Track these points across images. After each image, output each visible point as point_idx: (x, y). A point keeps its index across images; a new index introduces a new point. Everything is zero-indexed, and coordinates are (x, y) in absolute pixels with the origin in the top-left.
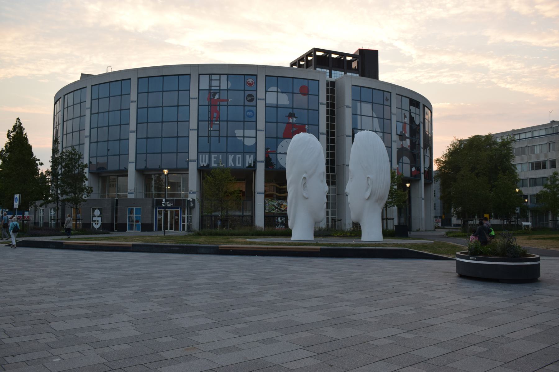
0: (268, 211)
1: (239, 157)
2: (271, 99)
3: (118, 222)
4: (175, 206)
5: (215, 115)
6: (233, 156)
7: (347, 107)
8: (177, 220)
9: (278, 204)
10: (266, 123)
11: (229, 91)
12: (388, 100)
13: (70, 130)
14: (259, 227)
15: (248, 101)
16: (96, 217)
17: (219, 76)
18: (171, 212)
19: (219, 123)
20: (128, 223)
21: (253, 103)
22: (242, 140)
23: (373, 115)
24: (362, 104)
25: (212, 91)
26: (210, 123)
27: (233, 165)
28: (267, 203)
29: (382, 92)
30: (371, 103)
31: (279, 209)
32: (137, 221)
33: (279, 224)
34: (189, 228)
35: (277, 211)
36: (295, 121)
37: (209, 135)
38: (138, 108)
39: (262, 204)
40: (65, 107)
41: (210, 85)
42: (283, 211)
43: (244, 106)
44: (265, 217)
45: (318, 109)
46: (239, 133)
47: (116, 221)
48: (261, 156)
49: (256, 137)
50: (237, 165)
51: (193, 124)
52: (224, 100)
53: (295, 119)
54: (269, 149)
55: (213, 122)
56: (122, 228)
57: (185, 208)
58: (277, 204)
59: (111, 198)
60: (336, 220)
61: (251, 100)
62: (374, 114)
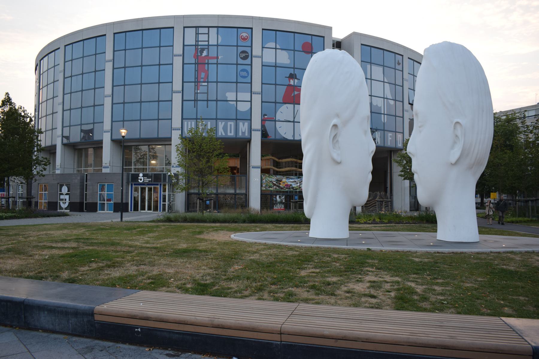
0: (264, 189)
1: (231, 125)
2: (269, 57)
3: (88, 201)
4: (154, 182)
5: (203, 75)
6: (223, 123)
8: (156, 199)
9: (276, 180)
10: (263, 103)
11: (219, 47)
13: (45, 99)
14: (254, 209)
15: (241, 58)
16: (63, 195)
17: (207, 29)
18: (150, 189)
19: (208, 84)
20: (98, 202)
21: (248, 61)
22: (234, 104)
23: (384, 80)
25: (199, 47)
26: (196, 84)
27: (224, 134)
28: (264, 179)
29: (394, 54)
30: (382, 66)
31: (278, 186)
32: (108, 200)
34: (170, 207)
35: (276, 189)
36: (297, 83)
37: (196, 99)
38: (114, 68)
39: (258, 180)
40: (41, 73)
41: (197, 40)
42: (282, 188)
43: (237, 64)
44: (261, 195)
46: (231, 96)
47: (86, 201)
48: (257, 123)
49: (251, 101)
50: (229, 134)
51: (177, 85)
52: (213, 58)
53: (296, 80)
54: (266, 115)
55: (201, 83)
56: (92, 208)
61: (245, 58)
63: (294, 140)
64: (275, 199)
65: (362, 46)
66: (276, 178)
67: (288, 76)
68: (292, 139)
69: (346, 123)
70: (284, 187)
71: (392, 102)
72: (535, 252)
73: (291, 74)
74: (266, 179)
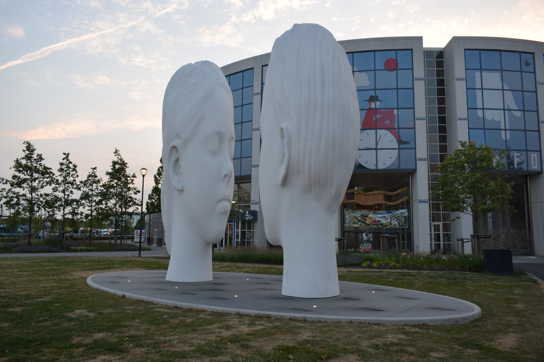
0: (348, 225)
7: (459, 79)
8: (231, 236)
9: (361, 216)
12: (530, 64)
24: (483, 73)
29: (518, 54)
31: (363, 222)
33: (364, 243)
36: (379, 105)
42: (368, 225)
45: (412, 87)
53: (378, 103)
57: (239, 221)
58: (359, 216)
60: (465, 241)
64: (360, 237)
66: (360, 213)
67: (368, 99)
68: (375, 168)
70: (371, 223)
71: (518, 114)
72: (308, 319)
73: (372, 97)
74: (350, 215)
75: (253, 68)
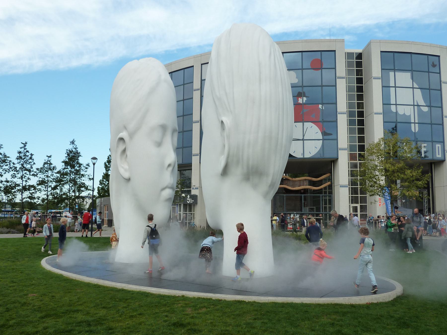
12: (436, 65)
23: (413, 86)
53: (305, 99)
59: (358, 205)
62: (415, 84)
63: (304, 158)
65: (382, 53)
68: (302, 157)
69: (131, 136)
75: (193, 66)
